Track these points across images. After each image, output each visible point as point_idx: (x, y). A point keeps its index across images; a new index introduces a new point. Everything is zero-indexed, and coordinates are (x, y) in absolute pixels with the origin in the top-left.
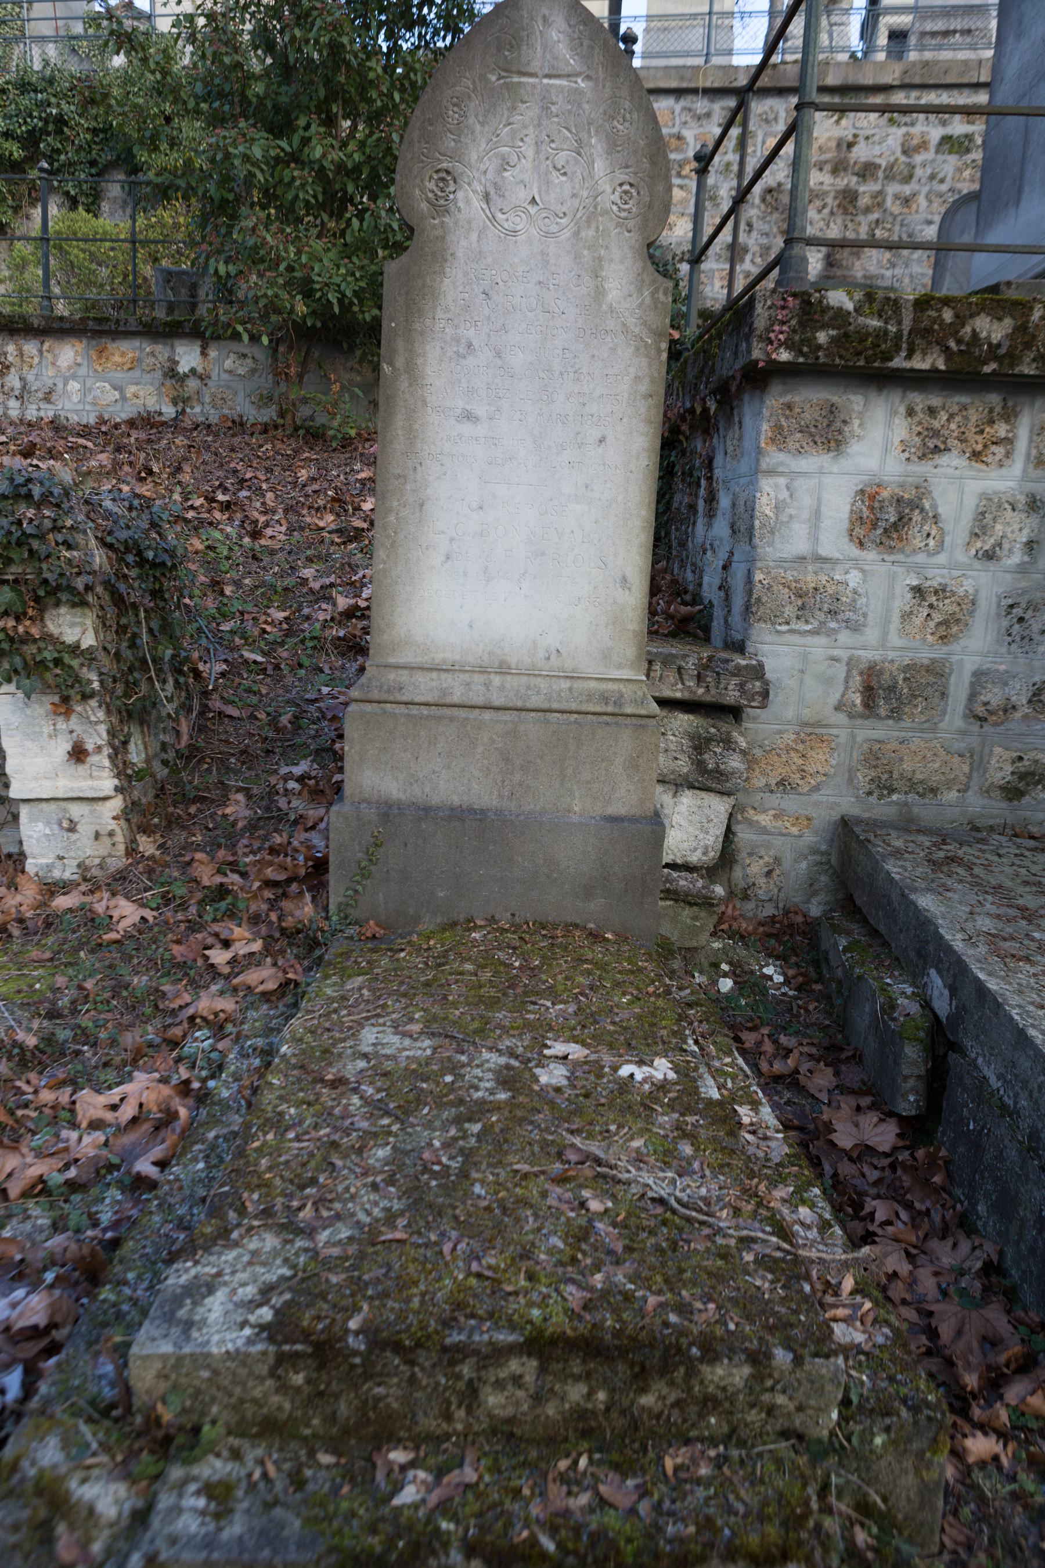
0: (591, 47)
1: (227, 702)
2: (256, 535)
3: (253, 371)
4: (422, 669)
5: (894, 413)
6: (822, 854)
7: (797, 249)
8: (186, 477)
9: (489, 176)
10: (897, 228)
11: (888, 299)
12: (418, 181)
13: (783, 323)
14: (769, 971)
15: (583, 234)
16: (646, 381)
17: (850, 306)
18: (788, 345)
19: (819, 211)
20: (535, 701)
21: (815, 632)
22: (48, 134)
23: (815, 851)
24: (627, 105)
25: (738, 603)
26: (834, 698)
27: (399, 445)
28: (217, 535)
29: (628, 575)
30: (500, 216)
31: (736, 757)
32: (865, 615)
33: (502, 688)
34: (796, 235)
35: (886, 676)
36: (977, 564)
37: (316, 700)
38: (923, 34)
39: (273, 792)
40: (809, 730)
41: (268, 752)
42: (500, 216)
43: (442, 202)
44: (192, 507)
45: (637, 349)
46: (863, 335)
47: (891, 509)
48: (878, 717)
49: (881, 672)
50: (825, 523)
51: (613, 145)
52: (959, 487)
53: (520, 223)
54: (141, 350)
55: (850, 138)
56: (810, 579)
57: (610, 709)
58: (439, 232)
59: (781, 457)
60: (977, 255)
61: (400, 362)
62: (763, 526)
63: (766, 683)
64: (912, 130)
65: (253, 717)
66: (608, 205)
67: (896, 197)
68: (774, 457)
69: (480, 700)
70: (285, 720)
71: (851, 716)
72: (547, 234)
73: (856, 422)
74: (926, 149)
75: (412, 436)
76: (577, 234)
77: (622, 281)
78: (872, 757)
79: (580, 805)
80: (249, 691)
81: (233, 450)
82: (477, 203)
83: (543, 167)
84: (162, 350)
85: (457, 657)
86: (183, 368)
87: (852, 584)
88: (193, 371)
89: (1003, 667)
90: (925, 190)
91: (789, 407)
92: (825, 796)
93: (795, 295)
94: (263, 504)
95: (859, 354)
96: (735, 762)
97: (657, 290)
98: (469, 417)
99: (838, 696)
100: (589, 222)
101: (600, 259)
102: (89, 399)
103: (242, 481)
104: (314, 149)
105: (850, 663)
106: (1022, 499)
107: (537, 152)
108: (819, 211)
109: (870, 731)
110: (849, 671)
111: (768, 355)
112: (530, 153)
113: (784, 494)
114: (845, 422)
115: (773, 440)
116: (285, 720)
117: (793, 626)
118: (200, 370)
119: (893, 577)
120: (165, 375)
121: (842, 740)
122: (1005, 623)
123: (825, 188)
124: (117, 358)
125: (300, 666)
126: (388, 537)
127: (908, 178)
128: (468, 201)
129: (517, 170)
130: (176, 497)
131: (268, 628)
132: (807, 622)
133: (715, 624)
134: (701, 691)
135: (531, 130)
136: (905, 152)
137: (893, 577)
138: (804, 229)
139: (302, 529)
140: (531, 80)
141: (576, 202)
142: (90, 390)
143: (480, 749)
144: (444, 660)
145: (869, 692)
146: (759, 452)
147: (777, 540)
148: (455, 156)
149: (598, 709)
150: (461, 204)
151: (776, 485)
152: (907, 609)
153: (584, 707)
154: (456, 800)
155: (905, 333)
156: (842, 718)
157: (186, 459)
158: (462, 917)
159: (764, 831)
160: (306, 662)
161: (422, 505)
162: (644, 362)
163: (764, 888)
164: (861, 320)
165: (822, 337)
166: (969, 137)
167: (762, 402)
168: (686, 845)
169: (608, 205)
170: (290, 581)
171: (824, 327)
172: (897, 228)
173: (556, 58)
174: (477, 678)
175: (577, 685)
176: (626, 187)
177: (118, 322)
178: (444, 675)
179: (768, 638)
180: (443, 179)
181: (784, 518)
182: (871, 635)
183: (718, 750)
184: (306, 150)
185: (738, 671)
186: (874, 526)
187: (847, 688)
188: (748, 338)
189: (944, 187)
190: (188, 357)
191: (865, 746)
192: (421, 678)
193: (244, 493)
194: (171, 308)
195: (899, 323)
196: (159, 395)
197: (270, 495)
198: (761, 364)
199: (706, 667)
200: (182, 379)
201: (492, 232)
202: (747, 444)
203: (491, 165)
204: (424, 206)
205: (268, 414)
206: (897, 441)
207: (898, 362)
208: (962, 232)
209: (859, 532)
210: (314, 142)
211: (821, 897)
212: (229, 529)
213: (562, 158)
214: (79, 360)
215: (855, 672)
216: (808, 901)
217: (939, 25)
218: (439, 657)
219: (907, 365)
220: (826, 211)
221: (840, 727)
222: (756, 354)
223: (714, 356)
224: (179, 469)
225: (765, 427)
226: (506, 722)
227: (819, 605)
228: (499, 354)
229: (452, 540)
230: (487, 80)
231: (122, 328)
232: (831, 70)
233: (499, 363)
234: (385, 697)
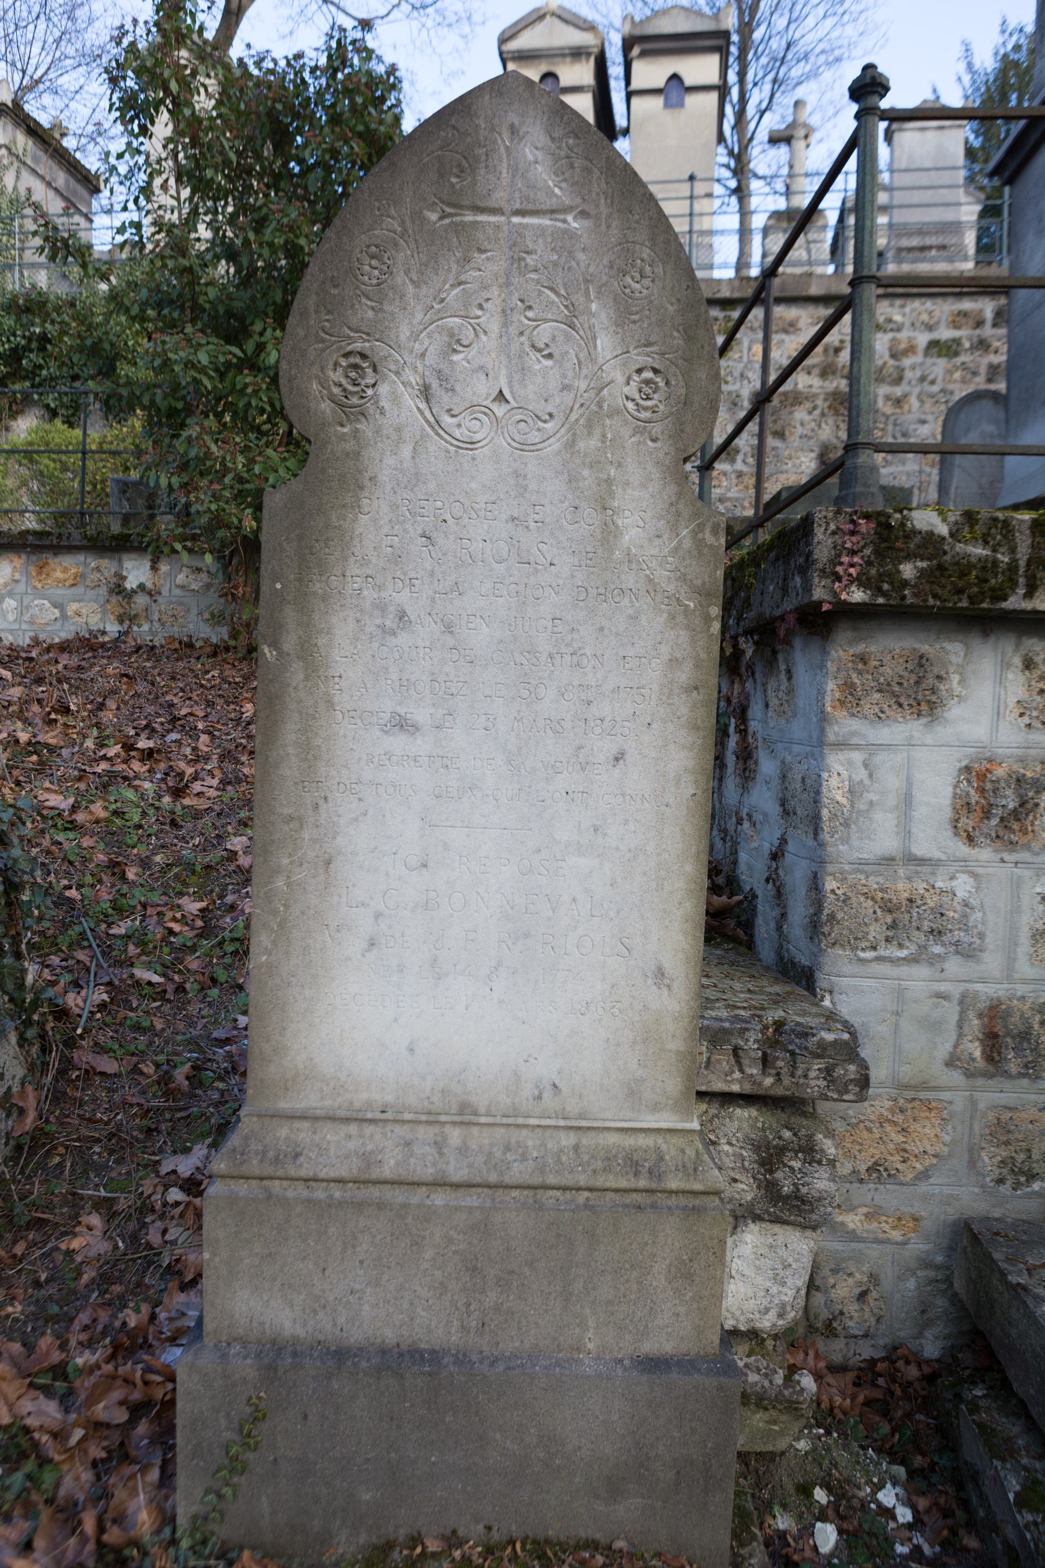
0: (588, 170)
1: (99, 1049)
2: (178, 793)
3: (208, 586)
4: (332, 1119)
5: (1006, 665)
6: (937, 1268)
7: (863, 457)
8: (108, 716)
9: (430, 360)
10: (890, 428)
11: (995, 520)
12: (315, 370)
13: (853, 553)
14: (888, 1497)
15: (581, 445)
16: (688, 666)
17: (943, 530)
18: (863, 581)
19: (810, 413)
20: (519, 1172)
21: (912, 960)
22: (32, 351)
23: (926, 1264)
24: (646, 253)
25: (799, 912)
26: (944, 1049)
27: (290, 770)
28: (130, 794)
29: (667, 965)
30: (446, 420)
31: (823, 1172)
32: (981, 936)
33: (463, 1150)
34: (861, 439)
35: (1015, 1019)
37: (227, 1041)
38: (900, 250)
39: (145, 1208)
40: (910, 1094)
41: (149, 1130)
42: (446, 420)
43: (355, 400)
44: (104, 758)
45: (672, 617)
46: (964, 567)
47: (1009, 792)
48: (1007, 1075)
49: (1008, 1013)
50: (920, 812)
51: (625, 313)
53: (481, 429)
54: (86, 565)
55: (837, 344)
56: (902, 888)
57: (643, 1183)
58: (350, 446)
59: (855, 725)
60: (1008, 458)
61: (290, 643)
62: (834, 817)
63: (864, 1066)
64: (899, 335)
65: (136, 1070)
66: (620, 401)
67: (887, 398)
68: (844, 725)
69: (428, 1173)
70: (180, 1075)
71: (969, 1074)
72: (523, 446)
73: (955, 678)
74: (914, 353)
75: (310, 755)
76: (571, 444)
77: (643, 516)
78: (1002, 1130)
79: (595, 1339)
80: (137, 1028)
81: (173, 678)
82: (410, 402)
83: (515, 347)
84: (107, 566)
85: (390, 1098)
86: (131, 584)
87: (961, 894)
88: (142, 587)
90: (916, 391)
91: (863, 659)
92: (938, 1186)
93: (867, 516)
94: (195, 749)
95: (960, 592)
96: (821, 1182)
97: (701, 527)
98: (402, 725)
99: (949, 1047)
100: (589, 426)
101: (609, 481)
102: (26, 618)
103: (175, 719)
104: (269, 354)
105: (965, 1001)
107: (505, 324)
108: (810, 413)
109: (996, 1095)
110: (962, 1013)
111: (835, 594)
112: (492, 323)
113: (862, 774)
114: (939, 677)
115: (842, 703)
116: (180, 1075)
117: (882, 952)
118: (149, 585)
119: (1017, 884)
120: (111, 592)
123: (814, 390)
124: (59, 574)
125: (214, 981)
126: (275, 912)
127: (898, 380)
128: (396, 399)
129: (473, 352)
130: (89, 743)
131: (176, 927)
132: (900, 946)
133: (759, 921)
134: (769, 1081)
135: (494, 292)
136: (893, 356)
137: (1017, 884)
138: (870, 432)
139: (239, 781)
140: (492, 219)
141: (569, 398)
142: (28, 607)
143: (429, 1254)
144: (369, 1105)
145: (992, 1041)
146: (824, 718)
147: (854, 835)
148: (375, 331)
149: (623, 1183)
150: (384, 403)
151: (850, 763)
153: (600, 1181)
154: (389, 1336)
155: (1022, 563)
156: (956, 1077)
157: (114, 692)
158: (402, 1534)
159: (853, 1236)
160: (222, 976)
161: (328, 863)
162: (684, 636)
163: (855, 1318)
164: (960, 547)
165: (908, 570)
166: (957, 341)
167: (824, 652)
168: (752, 1305)
169: (620, 401)
170: (215, 856)
171: (909, 557)
172: (890, 428)
173: (532, 187)
174: (425, 1133)
175: (587, 1140)
176: (648, 375)
177: (60, 536)
178: (369, 1129)
179: (847, 969)
180: (355, 367)
181: (862, 806)
182: (992, 962)
183: (796, 1164)
184: (263, 355)
185: (822, 1050)
186: (987, 814)
187: (960, 1036)
188: (804, 570)
189: (935, 389)
190: (136, 572)
191: (991, 1116)
192: (331, 1135)
193: (174, 736)
194: (126, 519)
195: (1013, 550)
196: (104, 612)
197: (204, 738)
198: (826, 607)
199: (774, 1043)
200: (130, 595)
201: (435, 444)
202: (801, 701)
203: (432, 345)
204: (326, 407)
205: (219, 634)
206: (1012, 701)
207: (1015, 602)
208: (968, 430)
209: (967, 822)
210: (269, 347)
211: (939, 1328)
212: (147, 785)
213: (544, 333)
214: (17, 576)
215: (971, 1014)
216: (920, 1335)
217: (915, 242)
218: (360, 1098)
219: (1027, 605)
220: (817, 412)
221: (954, 1090)
222: (818, 593)
223: (750, 587)
224: (101, 707)
225: (831, 686)
226: (470, 1209)
227: (915, 922)
228: (449, 629)
229: (378, 916)
230: (423, 219)
231: (64, 543)
232: (814, 281)
233: (450, 641)
234: (270, 1170)
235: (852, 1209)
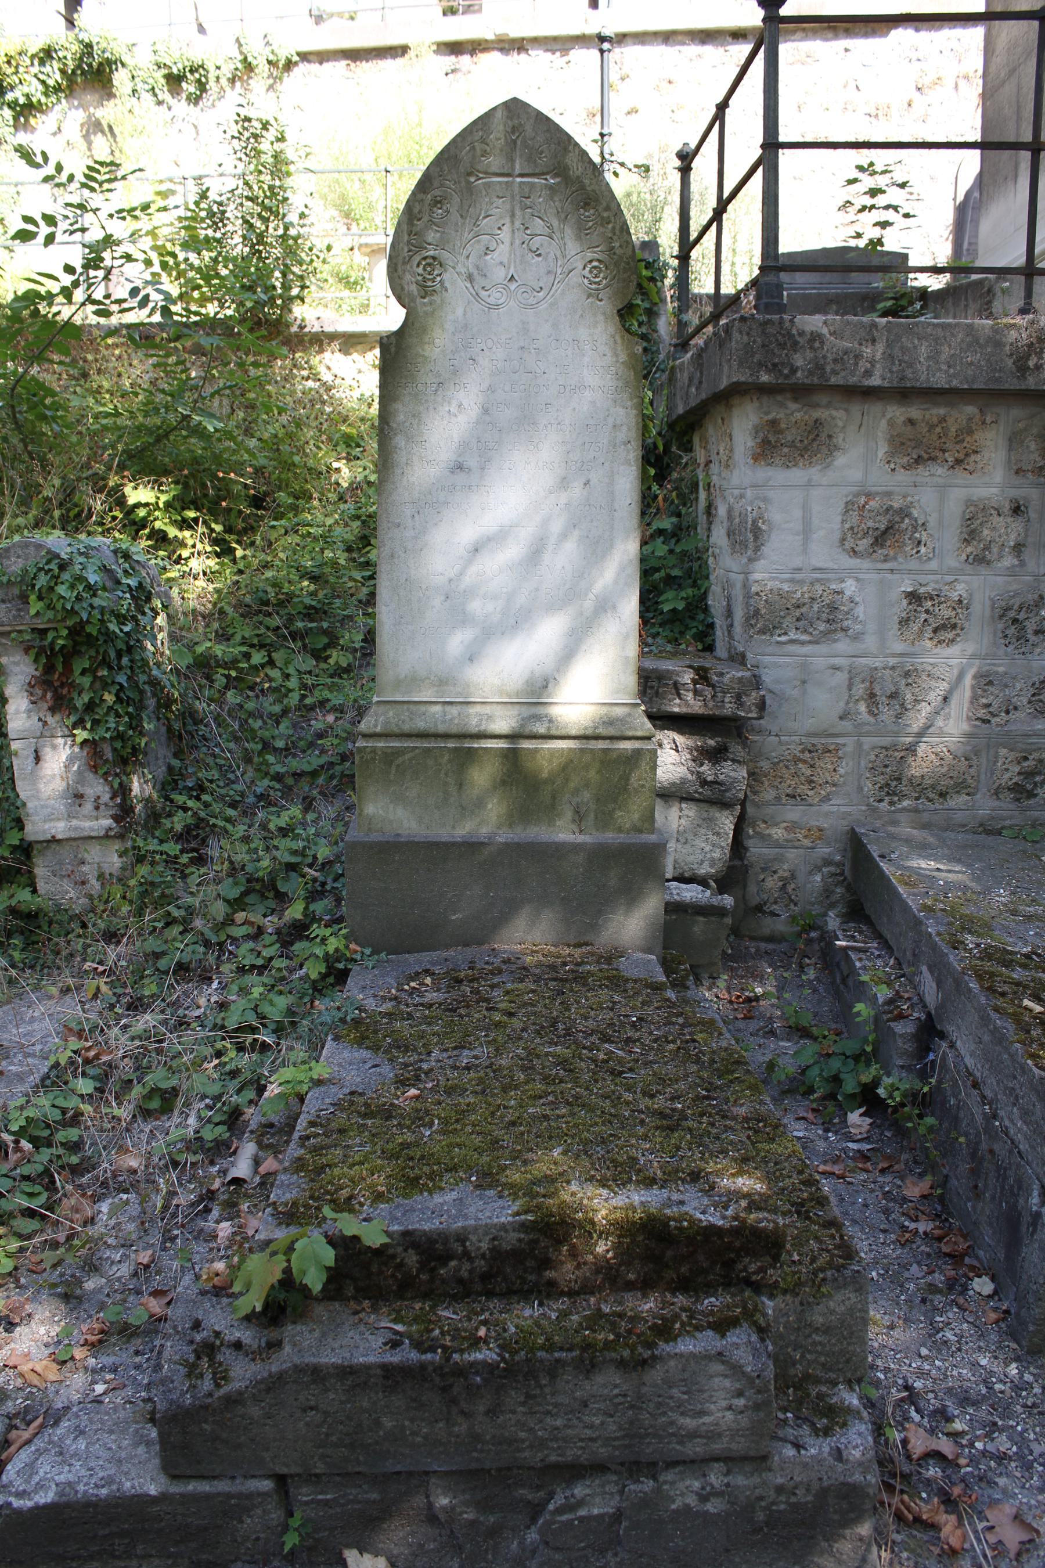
6: (838, 864)
23: (828, 862)
30: (483, 294)
36: (968, 568)
42: (483, 294)
43: (430, 284)
52: (939, 498)
87: (848, 593)
89: (1001, 669)
106: (1007, 507)
121: (849, 749)
122: (1000, 626)
152: (904, 615)
180: (429, 265)
182: (870, 642)
233: (488, 419)
235: (776, 825)
